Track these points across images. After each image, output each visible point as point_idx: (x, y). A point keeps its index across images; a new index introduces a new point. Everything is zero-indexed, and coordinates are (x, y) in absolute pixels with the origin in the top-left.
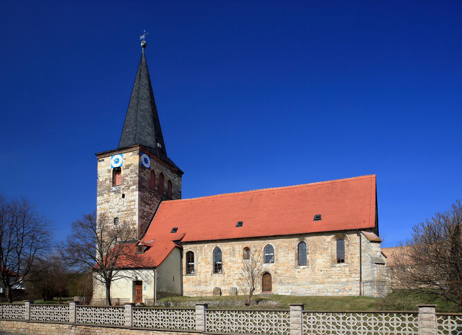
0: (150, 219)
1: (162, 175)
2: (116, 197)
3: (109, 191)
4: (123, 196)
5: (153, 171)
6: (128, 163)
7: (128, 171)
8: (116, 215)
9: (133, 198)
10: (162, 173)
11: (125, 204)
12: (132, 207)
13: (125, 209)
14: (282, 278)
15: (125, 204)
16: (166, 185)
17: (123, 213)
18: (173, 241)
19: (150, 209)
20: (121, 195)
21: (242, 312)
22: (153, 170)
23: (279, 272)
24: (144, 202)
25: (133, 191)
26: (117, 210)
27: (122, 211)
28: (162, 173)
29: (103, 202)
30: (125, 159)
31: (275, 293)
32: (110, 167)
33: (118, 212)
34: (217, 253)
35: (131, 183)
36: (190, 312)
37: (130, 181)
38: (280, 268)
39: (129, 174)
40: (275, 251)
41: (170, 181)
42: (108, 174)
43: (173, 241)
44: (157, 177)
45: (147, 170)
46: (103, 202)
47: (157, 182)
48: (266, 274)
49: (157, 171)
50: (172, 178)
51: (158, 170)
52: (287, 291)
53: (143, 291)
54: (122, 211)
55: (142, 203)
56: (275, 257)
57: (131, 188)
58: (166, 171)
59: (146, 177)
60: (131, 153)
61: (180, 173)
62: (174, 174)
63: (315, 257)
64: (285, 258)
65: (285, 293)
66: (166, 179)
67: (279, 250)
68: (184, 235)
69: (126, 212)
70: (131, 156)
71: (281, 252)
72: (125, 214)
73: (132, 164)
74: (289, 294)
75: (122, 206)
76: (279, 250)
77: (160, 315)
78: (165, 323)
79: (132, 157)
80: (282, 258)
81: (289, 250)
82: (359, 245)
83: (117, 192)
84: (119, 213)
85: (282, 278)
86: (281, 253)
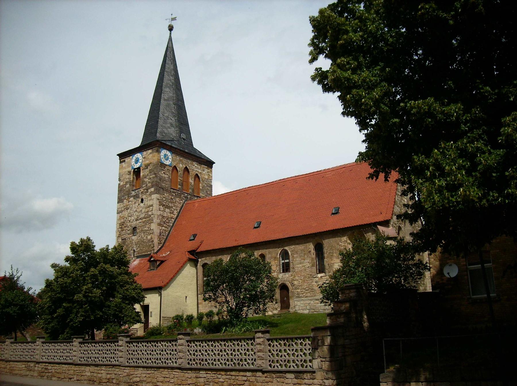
0: (171, 225)
1: (186, 169)
2: (135, 203)
3: (128, 197)
4: (142, 201)
5: (175, 168)
6: (147, 162)
7: (147, 172)
8: (134, 224)
9: (150, 203)
10: (186, 167)
11: (143, 210)
12: (150, 213)
13: (142, 216)
14: (299, 290)
15: (143, 210)
16: (191, 181)
17: (140, 221)
18: (188, 252)
19: (170, 213)
20: (140, 200)
21: (216, 342)
22: (175, 166)
23: (296, 283)
24: (163, 205)
25: (152, 193)
26: (136, 217)
27: (140, 219)
28: (186, 167)
29: (123, 209)
30: (144, 158)
31: (296, 313)
32: (131, 168)
33: (137, 220)
34: (285, 255)
35: (150, 184)
36: (250, 342)
37: (149, 182)
38: (297, 278)
39: (148, 175)
40: (291, 257)
41: (197, 174)
42: (128, 176)
43: (188, 252)
44: (181, 172)
45: (167, 168)
46: (123, 209)
47: (180, 179)
48: (284, 288)
49: (181, 167)
50: (200, 171)
51: (181, 165)
52: (305, 308)
53: (150, 318)
54: (140, 219)
55: (161, 207)
56: (291, 264)
57: (149, 191)
58: (192, 164)
59: (166, 176)
60: (150, 151)
61: (209, 164)
62: (203, 166)
63: (332, 262)
64: (301, 265)
65: (303, 310)
66: (192, 173)
67: (295, 256)
68: (202, 242)
69: (144, 220)
70: (150, 153)
71: (297, 257)
72: (143, 222)
73: (151, 163)
74: (306, 312)
75: (140, 213)
76: (295, 256)
77: (275, 348)
78: (298, 358)
79: (151, 155)
80: (298, 266)
81: (305, 254)
82: (196, 276)
83: (136, 197)
84: (138, 222)
85: (299, 290)
86: (297, 259)
